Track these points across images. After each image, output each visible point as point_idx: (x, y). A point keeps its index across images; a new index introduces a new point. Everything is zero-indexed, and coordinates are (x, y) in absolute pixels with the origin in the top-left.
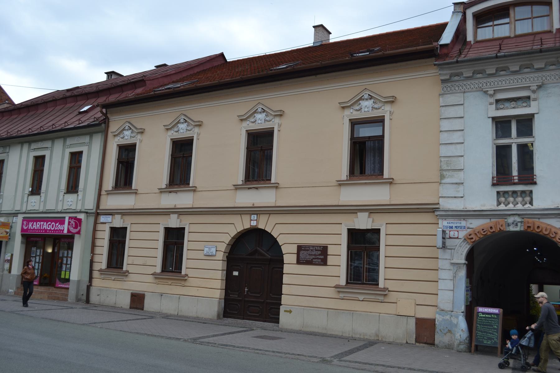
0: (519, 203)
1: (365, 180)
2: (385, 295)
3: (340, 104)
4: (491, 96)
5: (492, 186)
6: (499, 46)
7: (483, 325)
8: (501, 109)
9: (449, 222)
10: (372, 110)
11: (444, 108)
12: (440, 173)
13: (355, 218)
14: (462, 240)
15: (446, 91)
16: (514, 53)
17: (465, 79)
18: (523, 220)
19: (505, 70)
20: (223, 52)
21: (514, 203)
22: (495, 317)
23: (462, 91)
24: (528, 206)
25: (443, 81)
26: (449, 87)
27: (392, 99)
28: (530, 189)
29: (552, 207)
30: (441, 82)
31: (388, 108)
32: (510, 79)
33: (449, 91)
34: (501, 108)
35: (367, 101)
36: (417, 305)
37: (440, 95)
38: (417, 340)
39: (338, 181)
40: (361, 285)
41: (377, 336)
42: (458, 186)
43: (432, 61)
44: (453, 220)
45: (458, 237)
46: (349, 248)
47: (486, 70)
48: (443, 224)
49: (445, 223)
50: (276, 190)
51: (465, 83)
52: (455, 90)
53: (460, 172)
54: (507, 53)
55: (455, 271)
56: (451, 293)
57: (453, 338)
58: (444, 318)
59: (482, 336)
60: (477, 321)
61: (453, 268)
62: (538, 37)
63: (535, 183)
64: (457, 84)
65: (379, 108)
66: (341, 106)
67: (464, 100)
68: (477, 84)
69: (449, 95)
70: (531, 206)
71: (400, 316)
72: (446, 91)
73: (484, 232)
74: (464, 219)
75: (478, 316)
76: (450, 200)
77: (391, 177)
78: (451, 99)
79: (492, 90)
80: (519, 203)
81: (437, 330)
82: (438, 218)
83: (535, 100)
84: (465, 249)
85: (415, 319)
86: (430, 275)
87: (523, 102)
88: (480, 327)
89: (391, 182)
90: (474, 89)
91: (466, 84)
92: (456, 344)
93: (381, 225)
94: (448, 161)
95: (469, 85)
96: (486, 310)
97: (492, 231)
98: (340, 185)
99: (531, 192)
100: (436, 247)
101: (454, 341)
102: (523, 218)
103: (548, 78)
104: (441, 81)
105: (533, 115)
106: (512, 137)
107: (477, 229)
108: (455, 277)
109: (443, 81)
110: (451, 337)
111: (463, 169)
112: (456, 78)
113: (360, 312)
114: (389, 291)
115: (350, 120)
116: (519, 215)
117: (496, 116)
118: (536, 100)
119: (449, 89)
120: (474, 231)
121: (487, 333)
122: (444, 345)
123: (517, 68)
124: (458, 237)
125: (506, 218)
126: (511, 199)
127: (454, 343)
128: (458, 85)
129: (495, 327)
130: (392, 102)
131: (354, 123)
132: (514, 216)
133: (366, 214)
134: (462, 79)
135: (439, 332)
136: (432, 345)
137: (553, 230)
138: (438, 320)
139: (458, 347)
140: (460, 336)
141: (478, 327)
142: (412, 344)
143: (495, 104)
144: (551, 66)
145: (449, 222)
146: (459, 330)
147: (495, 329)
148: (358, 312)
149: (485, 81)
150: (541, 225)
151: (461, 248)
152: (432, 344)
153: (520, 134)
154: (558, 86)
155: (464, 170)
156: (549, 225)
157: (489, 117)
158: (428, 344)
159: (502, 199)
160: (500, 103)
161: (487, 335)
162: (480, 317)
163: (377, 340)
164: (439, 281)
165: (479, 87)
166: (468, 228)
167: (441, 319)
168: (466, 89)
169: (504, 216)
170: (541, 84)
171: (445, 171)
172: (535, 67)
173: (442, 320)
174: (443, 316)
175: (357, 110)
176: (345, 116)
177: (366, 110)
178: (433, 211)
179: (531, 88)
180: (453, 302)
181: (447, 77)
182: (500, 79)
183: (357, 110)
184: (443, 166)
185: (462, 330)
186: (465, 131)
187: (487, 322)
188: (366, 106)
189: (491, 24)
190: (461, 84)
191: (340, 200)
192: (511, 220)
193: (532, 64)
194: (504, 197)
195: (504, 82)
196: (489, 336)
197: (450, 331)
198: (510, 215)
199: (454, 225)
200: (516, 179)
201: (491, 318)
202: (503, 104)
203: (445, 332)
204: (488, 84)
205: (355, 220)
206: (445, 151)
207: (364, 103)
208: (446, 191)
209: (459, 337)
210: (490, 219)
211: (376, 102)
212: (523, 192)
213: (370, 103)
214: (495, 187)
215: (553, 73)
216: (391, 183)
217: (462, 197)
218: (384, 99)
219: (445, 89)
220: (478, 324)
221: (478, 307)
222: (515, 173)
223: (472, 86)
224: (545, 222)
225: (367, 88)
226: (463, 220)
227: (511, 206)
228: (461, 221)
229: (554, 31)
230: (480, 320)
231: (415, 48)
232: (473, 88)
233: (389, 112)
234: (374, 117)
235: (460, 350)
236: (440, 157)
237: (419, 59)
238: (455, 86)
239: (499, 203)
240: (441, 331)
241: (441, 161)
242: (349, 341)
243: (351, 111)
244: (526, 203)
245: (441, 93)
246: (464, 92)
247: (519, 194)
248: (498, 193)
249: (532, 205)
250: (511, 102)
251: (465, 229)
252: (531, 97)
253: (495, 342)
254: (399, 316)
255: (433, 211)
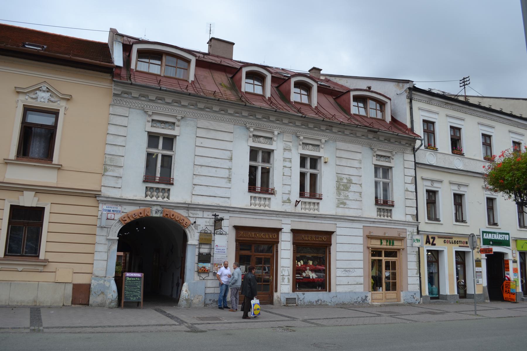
0: (154, 196)
1: (35, 163)
2: (45, 266)
3: (17, 88)
4: (150, 116)
5: (143, 182)
6: (186, 86)
7: (130, 286)
8: (154, 127)
9: (108, 206)
10: (48, 101)
11: (113, 116)
12: (104, 167)
13: (20, 196)
14: (117, 221)
15: (116, 103)
16: (173, 90)
17: (132, 98)
18: (163, 209)
19: (161, 100)
20: (191, 60)
21: (156, 196)
22: (139, 279)
23: (128, 106)
24: (166, 199)
25: (115, 95)
26: (119, 100)
27: (70, 97)
28: (169, 188)
29: (182, 202)
30: (113, 95)
31: (63, 104)
32: (161, 106)
33: (118, 104)
34: (154, 126)
35: (44, 93)
36: (74, 273)
37: (110, 105)
38: (73, 303)
39: (4, 159)
40: (36, 258)
41: (35, 301)
42: (117, 179)
43: (108, 76)
44: (111, 205)
45: (114, 219)
46: (10, 223)
47: (166, 99)
48: (103, 208)
49: (105, 207)
50: (58, 171)
51: (131, 101)
52: (123, 104)
53: (120, 169)
54: (168, 89)
55: (110, 245)
56: (105, 262)
57: (105, 298)
58: (99, 282)
59: (129, 295)
60: (125, 283)
61: (108, 243)
62: (159, 78)
63: (172, 184)
64: (125, 100)
65: (55, 102)
66: (17, 90)
67: (129, 114)
68: (140, 104)
69: (118, 107)
70: (168, 200)
71: (59, 283)
72: (116, 103)
73: (135, 216)
74: (120, 205)
75: (126, 279)
76: (110, 189)
77: (60, 164)
78: (119, 110)
79: (151, 112)
80: (154, 196)
81: (92, 292)
82: (99, 203)
83: (178, 126)
84: (118, 228)
85: (72, 285)
86: (88, 248)
87: (170, 126)
88: (128, 288)
89: (59, 168)
90: (138, 108)
91: (132, 102)
92: (107, 302)
93: (47, 204)
94: (112, 158)
95: (134, 103)
96: (132, 275)
97: (141, 216)
98: (6, 163)
99: (169, 190)
100: (96, 225)
101: (106, 300)
102: (163, 208)
103: (188, 113)
104: (113, 94)
105: (175, 136)
106: (159, 149)
107: (130, 214)
108: (110, 250)
109: (115, 95)
110: (104, 297)
111: (122, 167)
112: (126, 95)
113: (18, 282)
114: (48, 262)
115: (24, 105)
116: (160, 205)
117: (151, 131)
118: (179, 126)
119: (118, 102)
120: (128, 215)
121: (133, 292)
122: (97, 304)
123: (170, 101)
124: (114, 219)
125: (151, 207)
126: (155, 193)
127: (106, 302)
128: (126, 101)
129: (139, 287)
130: (68, 100)
131: (27, 109)
132: (157, 206)
133: (34, 193)
134: (130, 97)
135: (94, 294)
136: (86, 305)
137: (182, 218)
138: (93, 284)
139: (110, 304)
140: (112, 296)
141: (126, 288)
142: (69, 306)
143: (151, 122)
144: (191, 106)
145: (108, 206)
146: (112, 291)
147: (138, 288)
148: (15, 282)
149: (146, 103)
150: (175, 214)
151: (116, 227)
152: (87, 304)
153: (263, 161)
154: (193, 120)
155: (123, 167)
156: (179, 214)
157: (146, 131)
158: (82, 304)
159: (149, 193)
160: (154, 122)
161: (133, 294)
162: (127, 280)
163: (34, 305)
164: (96, 253)
165: (141, 107)
166: (122, 212)
167: (96, 284)
168: (131, 106)
169: (150, 205)
170: (184, 116)
171: (108, 166)
172: (182, 104)
173: (97, 284)
174: (98, 281)
175: (32, 98)
176: (20, 101)
177: (42, 100)
178: (95, 196)
179: (177, 117)
180: (106, 269)
181: (119, 93)
182: (157, 105)
183: (32, 98)
184: (107, 161)
185: (114, 291)
186: (127, 137)
187: (133, 284)
188: (43, 97)
189: (147, 60)
190: (128, 100)
191: (5, 177)
192: (154, 208)
193: (180, 101)
194: (150, 191)
195: (159, 108)
196: (134, 294)
197: (102, 293)
198: (154, 205)
199: (112, 209)
200: (157, 179)
201: (136, 280)
202: (156, 124)
203: (99, 293)
204: (148, 107)
205: (21, 197)
206: (109, 150)
207: (40, 94)
208: (106, 181)
209: (111, 297)
210: (203, 211)
211: (52, 96)
212: (164, 189)
213: (47, 95)
214: (145, 183)
215: (191, 111)
216: (59, 169)
217: (120, 188)
218: (62, 96)
219: (115, 101)
220: (126, 286)
221: (126, 273)
222: (158, 175)
223: (136, 105)
224: (177, 212)
225: (46, 81)
226: (119, 205)
227: (154, 198)
228: (117, 207)
229: (190, 82)
230: (127, 282)
231: (98, 62)
232: (136, 106)
233: (64, 107)
234: (28, 105)
235: (112, 307)
236: (105, 154)
237: (97, 71)
238: (124, 101)
239: (146, 196)
240: (95, 293)
241: (106, 158)
242: (12, 309)
243: (27, 97)
244: (165, 197)
245: (112, 104)
246: (130, 108)
247: (160, 190)
248: (147, 187)
249: (169, 200)
250: (162, 123)
251: (120, 213)
252: (176, 124)
253: (139, 299)
254: (57, 283)
255: (95, 196)
